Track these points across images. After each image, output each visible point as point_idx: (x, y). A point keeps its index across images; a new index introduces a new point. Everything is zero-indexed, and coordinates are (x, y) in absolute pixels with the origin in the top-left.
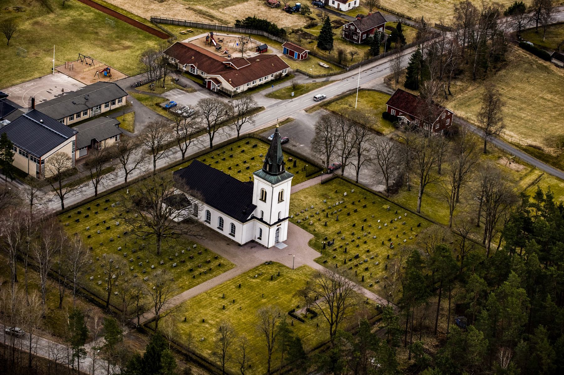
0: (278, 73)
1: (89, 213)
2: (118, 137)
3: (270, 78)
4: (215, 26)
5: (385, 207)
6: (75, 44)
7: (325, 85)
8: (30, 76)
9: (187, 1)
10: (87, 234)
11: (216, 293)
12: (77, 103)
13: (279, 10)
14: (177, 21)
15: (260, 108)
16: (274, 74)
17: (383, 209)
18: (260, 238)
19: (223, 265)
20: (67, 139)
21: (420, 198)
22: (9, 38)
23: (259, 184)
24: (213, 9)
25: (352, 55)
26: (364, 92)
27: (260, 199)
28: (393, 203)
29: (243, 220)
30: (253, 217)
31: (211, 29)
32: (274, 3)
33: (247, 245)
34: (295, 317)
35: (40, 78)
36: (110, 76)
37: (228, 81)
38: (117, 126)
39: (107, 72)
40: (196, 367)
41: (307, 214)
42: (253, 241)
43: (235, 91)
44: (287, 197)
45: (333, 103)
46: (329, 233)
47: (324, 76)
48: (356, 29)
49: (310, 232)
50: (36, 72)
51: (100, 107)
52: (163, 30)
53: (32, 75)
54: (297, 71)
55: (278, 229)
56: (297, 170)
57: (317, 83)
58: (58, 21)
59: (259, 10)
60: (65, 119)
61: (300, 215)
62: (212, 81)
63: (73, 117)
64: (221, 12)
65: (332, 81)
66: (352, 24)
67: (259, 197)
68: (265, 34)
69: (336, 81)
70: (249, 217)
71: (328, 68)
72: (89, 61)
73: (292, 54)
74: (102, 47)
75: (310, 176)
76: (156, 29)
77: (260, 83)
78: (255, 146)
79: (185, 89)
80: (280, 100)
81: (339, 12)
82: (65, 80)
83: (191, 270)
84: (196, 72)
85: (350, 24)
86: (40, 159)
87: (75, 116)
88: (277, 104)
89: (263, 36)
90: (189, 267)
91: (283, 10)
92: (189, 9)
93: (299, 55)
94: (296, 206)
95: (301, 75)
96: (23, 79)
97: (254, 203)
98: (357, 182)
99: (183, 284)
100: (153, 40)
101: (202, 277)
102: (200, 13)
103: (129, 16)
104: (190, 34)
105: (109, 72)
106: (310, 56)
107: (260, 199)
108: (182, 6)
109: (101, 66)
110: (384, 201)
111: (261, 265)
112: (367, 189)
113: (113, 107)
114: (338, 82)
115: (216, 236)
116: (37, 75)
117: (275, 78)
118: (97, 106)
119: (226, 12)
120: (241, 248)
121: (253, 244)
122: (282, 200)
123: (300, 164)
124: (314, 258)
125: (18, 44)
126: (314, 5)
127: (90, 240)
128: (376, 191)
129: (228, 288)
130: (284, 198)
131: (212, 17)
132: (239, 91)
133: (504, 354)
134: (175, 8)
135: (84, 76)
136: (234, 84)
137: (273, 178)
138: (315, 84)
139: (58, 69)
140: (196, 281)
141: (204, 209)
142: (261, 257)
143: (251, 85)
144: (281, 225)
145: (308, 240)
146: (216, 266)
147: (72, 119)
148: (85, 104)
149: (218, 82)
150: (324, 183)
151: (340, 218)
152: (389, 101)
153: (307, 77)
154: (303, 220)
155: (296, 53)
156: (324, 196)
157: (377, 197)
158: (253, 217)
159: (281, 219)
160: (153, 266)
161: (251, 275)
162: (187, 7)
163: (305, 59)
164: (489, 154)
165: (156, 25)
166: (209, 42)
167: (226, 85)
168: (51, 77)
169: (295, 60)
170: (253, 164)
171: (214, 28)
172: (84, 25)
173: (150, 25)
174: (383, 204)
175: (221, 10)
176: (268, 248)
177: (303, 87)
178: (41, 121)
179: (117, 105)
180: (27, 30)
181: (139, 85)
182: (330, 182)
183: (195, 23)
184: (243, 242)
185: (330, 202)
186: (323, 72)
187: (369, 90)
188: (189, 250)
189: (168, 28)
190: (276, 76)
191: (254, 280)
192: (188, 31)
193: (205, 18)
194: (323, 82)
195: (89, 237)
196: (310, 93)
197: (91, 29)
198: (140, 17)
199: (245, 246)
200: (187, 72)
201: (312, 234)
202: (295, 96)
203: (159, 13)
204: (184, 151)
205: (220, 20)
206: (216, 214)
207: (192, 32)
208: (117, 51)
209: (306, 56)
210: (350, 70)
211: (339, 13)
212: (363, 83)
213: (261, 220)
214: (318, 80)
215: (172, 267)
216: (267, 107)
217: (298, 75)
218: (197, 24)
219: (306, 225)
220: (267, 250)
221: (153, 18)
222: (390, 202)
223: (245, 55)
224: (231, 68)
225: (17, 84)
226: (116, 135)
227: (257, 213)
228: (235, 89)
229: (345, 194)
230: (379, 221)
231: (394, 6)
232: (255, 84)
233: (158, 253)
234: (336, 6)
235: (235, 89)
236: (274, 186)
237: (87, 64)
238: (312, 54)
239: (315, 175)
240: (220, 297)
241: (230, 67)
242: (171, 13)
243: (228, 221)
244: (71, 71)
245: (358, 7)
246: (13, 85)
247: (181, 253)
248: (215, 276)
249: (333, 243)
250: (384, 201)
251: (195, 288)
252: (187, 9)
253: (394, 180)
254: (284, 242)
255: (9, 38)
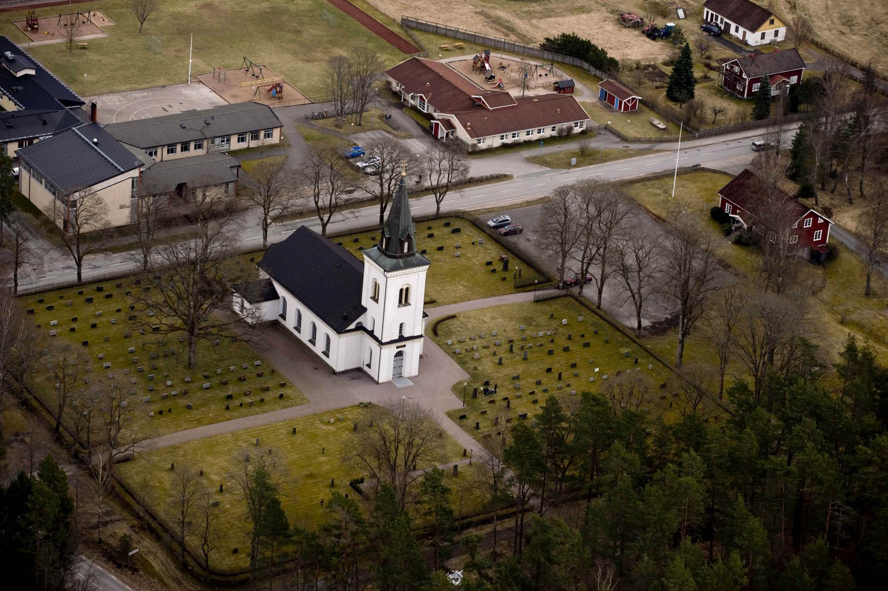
0: (565, 125)
1: (115, 292)
2: (231, 186)
3: (548, 132)
4: (515, 45)
5: (624, 350)
6: (253, 44)
7: (641, 155)
8: (148, 83)
9: (485, 2)
10: (93, 321)
11: (249, 437)
12: (188, 127)
13: (637, 33)
14: (444, 29)
15: (506, 176)
16: (558, 126)
17: (619, 353)
18: (326, 353)
19: (288, 397)
20: (123, 173)
21: (682, 342)
22: (143, 19)
23: (372, 272)
24: (522, 18)
25: (716, 112)
26: (705, 174)
27: (371, 298)
28: (640, 346)
29: (340, 330)
30: (360, 328)
31: (489, 46)
32: (631, 20)
33: (347, 375)
34: (359, 491)
35: (163, 87)
36: (280, 98)
37: (465, 127)
38: (235, 171)
39: (276, 90)
40: (151, 539)
41: (478, 344)
42: (359, 370)
43: (474, 145)
44: (417, 297)
45: (637, 184)
46: (499, 375)
47: (649, 141)
48: (741, 72)
49: (467, 370)
50: (162, 78)
51: (228, 140)
52: (414, 40)
53: (153, 81)
54: (607, 128)
55: (400, 354)
56: (506, 274)
57: (630, 150)
58: (246, 6)
59: (601, 28)
60: (159, 151)
61: (467, 342)
62: (440, 124)
63: (176, 149)
64: (532, 25)
65: (658, 151)
66: (736, 63)
67: (371, 294)
68: (586, 65)
69: (666, 151)
70: (353, 326)
71: (663, 129)
72: (257, 71)
73: (612, 100)
74: (295, 53)
75: (522, 287)
76: (403, 37)
77: (527, 138)
78: (456, 231)
79: (395, 132)
80: (548, 169)
81: (743, 46)
82: (202, 95)
83: (230, 397)
84: (426, 108)
85: (732, 63)
86: (69, 199)
87: (179, 147)
88: (538, 175)
89: (581, 68)
90: (230, 393)
91: (643, 32)
92: (482, 13)
93: (621, 102)
94: (467, 329)
95: (610, 135)
96: (133, 86)
97: (364, 303)
98: (599, 307)
99: (204, 416)
100: (388, 53)
101: (242, 410)
102: (497, 22)
103: (370, 13)
104: (457, 51)
105: (281, 92)
106: (644, 108)
107: (371, 298)
108: (471, 7)
109: (271, 79)
110: (626, 342)
111: (351, 407)
112: (611, 319)
113: (253, 144)
114: (667, 153)
115: (302, 352)
116: (161, 81)
117: (558, 133)
118: (223, 137)
119: (541, 25)
120: (335, 377)
121: (358, 374)
122: (407, 303)
123: (515, 266)
124: (447, 410)
125: (158, 33)
126: (704, 30)
127: (94, 330)
128: (624, 326)
129: (273, 433)
130: (412, 300)
131: (511, 29)
132: (483, 146)
133: (604, 575)
134: (456, 10)
135: (238, 93)
136: (473, 133)
137: (389, 262)
138: (626, 151)
139: (201, 78)
140: (227, 414)
141: (294, 304)
142: (361, 393)
143: (509, 140)
144: (404, 346)
145: (456, 381)
146: (275, 398)
147: (171, 151)
148: (201, 132)
149: (449, 125)
150: (538, 301)
151: (529, 356)
152: (724, 189)
153: (618, 140)
154: (466, 350)
155: (617, 99)
156: (528, 321)
157: (618, 333)
158: (360, 328)
159: (406, 336)
160: (169, 383)
161: (325, 419)
162: (478, 10)
163: (631, 110)
164: (874, 298)
165: (407, 32)
166: (479, 67)
167: (462, 133)
168: (183, 87)
169: (613, 112)
170: (436, 257)
171: (503, 46)
172: (285, 18)
173: (396, 30)
174: (622, 346)
175: (534, 21)
176: (378, 383)
177: (599, 152)
178: (95, 140)
179: (263, 141)
180: (187, 13)
181: (322, 116)
182: (551, 301)
183: (472, 35)
184: (339, 368)
185: (531, 330)
186: (652, 134)
187: (714, 171)
188: (245, 368)
189: (420, 37)
190: (561, 131)
191: (325, 427)
192: (456, 47)
193: (497, 30)
194: (642, 150)
195: (94, 326)
196: (608, 163)
197: (294, 25)
198: (387, 16)
199: (343, 376)
200: (414, 108)
201: (469, 373)
202: (577, 166)
203: (424, 14)
204: (325, 222)
205: (522, 37)
206: (309, 317)
207: (462, 48)
208: (316, 63)
209: (634, 107)
210: (700, 137)
211: (740, 48)
212: (710, 161)
213: (371, 333)
214: (633, 146)
215: (201, 389)
216: (518, 177)
217: (604, 134)
218: (446, 29)
219: (467, 359)
220: (374, 386)
221: (405, 20)
222: (635, 345)
223: (530, 93)
224: (481, 107)
225: (119, 92)
226: (227, 183)
227: (366, 320)
228: (475, 141)
229: (564, 321)
230: (597, 370)
231: (850, 48)
232: (516, 138)
233: (190, 364)
234: (740, 35)
235: (475, 141)
236: (389, 274)
237: (253, 75)
238: (649, 105)
239: (529, 288)
240: (251, 444)
241: (480, 105)
242: (447, 16)
243: (323, 329)
244: (219, 82)
245: (782, 42)
246: (113, 92)
247: (229, 369)
248: (264, 412)
249: (495, 392)
250: (626, 342)
251: (220, 424)
252: (476, 13)
253: (671, 314)
254: (410, 378)
255: (143, 19)
